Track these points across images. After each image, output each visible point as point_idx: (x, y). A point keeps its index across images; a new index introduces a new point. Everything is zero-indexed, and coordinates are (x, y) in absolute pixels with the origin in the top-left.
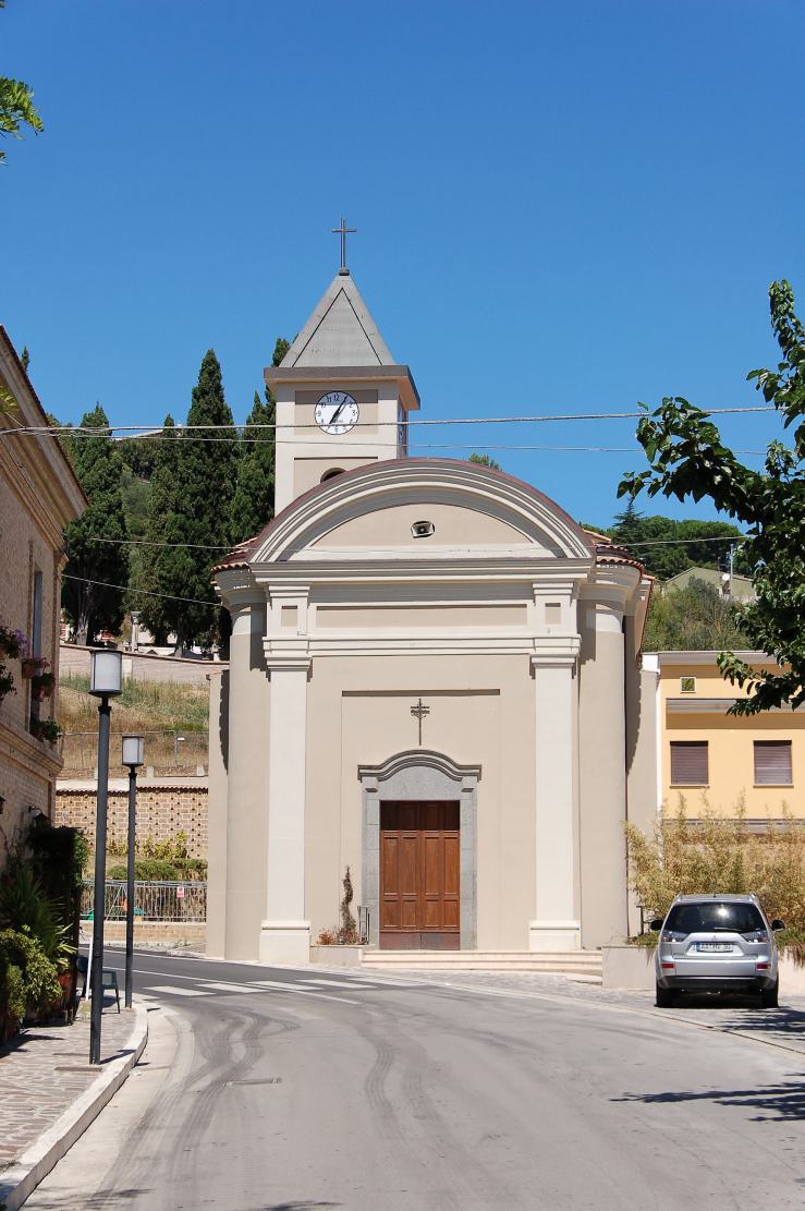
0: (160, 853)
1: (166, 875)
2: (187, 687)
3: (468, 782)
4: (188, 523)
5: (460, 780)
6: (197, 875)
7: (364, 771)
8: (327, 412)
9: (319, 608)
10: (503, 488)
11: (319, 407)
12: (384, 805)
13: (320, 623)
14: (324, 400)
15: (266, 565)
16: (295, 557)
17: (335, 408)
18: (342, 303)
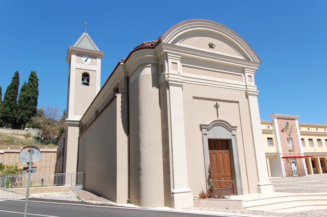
0: (10, 167)
1: (13, 173)
2: (7, 134)
4: (10, 102)
6: (20, 172)
7: (202, 127)
8: (84, 59)
9: (183, 66)
10: (234, 36)
11: (82, 58)
12: (210, 141)
13: (183, 71)
14: (83, 56)
15: (167, 44)
16: (178, 44)
17: (86, 58)
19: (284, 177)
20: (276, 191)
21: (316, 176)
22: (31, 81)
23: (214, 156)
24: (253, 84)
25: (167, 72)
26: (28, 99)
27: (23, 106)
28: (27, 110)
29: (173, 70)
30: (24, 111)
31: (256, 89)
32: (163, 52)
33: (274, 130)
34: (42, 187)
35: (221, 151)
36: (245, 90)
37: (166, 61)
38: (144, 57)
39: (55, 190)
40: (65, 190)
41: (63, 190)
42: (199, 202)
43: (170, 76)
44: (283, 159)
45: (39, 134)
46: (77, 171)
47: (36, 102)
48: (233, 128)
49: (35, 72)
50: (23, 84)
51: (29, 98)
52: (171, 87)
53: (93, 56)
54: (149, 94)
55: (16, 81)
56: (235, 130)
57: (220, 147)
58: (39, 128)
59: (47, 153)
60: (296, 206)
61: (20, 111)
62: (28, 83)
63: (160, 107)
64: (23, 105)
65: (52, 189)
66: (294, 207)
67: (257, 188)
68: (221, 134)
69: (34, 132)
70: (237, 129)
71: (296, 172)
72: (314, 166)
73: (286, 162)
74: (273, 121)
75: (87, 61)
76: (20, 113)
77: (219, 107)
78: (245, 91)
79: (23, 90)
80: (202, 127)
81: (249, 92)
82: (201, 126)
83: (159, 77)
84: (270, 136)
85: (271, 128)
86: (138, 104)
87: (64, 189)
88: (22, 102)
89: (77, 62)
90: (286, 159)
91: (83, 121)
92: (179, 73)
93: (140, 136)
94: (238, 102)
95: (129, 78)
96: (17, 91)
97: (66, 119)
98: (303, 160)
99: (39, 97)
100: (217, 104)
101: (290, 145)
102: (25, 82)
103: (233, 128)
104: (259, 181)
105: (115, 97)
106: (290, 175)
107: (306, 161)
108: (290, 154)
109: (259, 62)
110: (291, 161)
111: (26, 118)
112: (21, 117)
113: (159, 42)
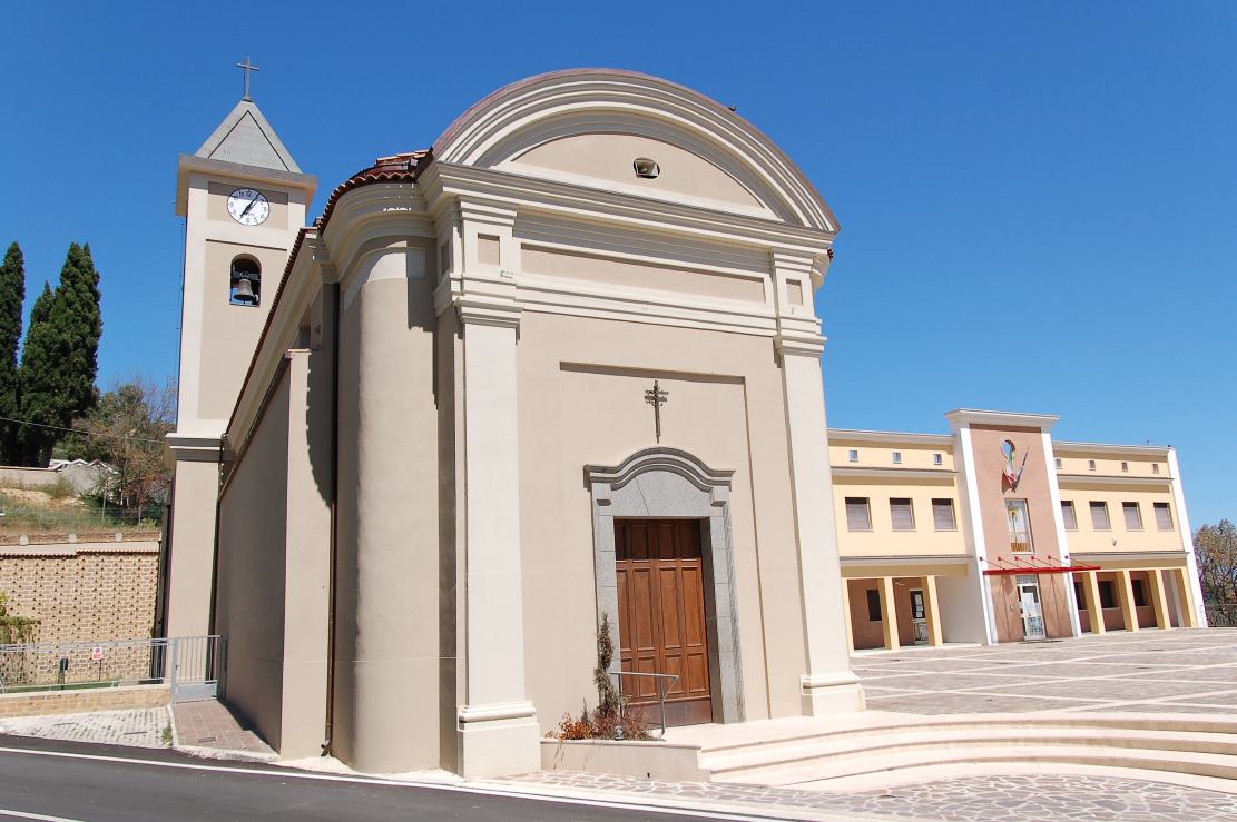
3: (719, 492)
5: (709, 491)
6: (17, 630)
7: (590, 476)
8: (239, 204)
9: (524, 246)
11: (231, 199)
12: (624, 527)
13: (526, 267)
15: (450, 165)
16: (506, 166)
17: (248, 202)
18: (248, 121)
19: (990, 643)
20: (871, 705)
21: (1114, 639)
22: (69, 283)
23: (641, 582)
24: (807, 310)
25: (456, 273)
26: (59, 350)
27: (40, 379)
28: (55, 394)
29: (485, 262)
30: (43, 395)
31: (818, 329)
32: (442, 196)
33: (960, 472)
34: (60, 692)
35: (671, 564)
36: (774, 333)
37: (455, 229)
38: (380, 213)
39: (110, 702)
40: (147, 702)
41: (143, 701)
42: (561, 752)
43: (468, 285)
44: (987, 577)
45: (103, 482)
46: (212, 631)
47: (93, 364)
48: (715, 479)
49: (86, 247)
50: (40, 292)
51: (64, 349)
52: (469, 328)
53: (273, 191)
54: (393, 349)
55: (9, 281)
56: (727, 484)
57: (664, 552)
58: (106, 458)
59: (121, 557)
60: (896, 765)
61: (29, 396)
62: (58, 290)
63: (436, 402)
64: (39, 376)
65: (100, 699)
66: (890, 766)
67: (802, 697)
68: (667, 499)
69: (83, 476)
70: (734, 479)
71: (1037, 623)
72: (1139, 601)
73: (999, 588)
74: (957, 436)
75: (251, 212)
76: (29, 404)
77: (665, 400)
78: (771, 339)
79: (39, 316)
80: (592, 474)
81: (785, 343)
82: (587, 470)
83: (439, 288)
84: (942, 492)
85: (948, 462)
86: (358, 391)
87: (143, 696)
88: (38, 363)
89: (213, 215)
90: (998, 578)
91: (232, 440)
92: (504, 274)
93: (360, 510)
94: (742, 380)
95: (342, 289)
96: (15, 320)
97: (169, 435)
98: (1067, 580)
99: (102, 343)
100: (656, 388)
101: (1021, 525)
102: (47, 286)
103: (715, 479)
104: (809, 671)
105: (285, 364)
106: (1013, 637)
107: (1076, 584)
108: (1017, 559)
109: (831, 229)
110: (1021, 586)
111: (53, 423)
112: (35, 419)
113: (427, 160)
